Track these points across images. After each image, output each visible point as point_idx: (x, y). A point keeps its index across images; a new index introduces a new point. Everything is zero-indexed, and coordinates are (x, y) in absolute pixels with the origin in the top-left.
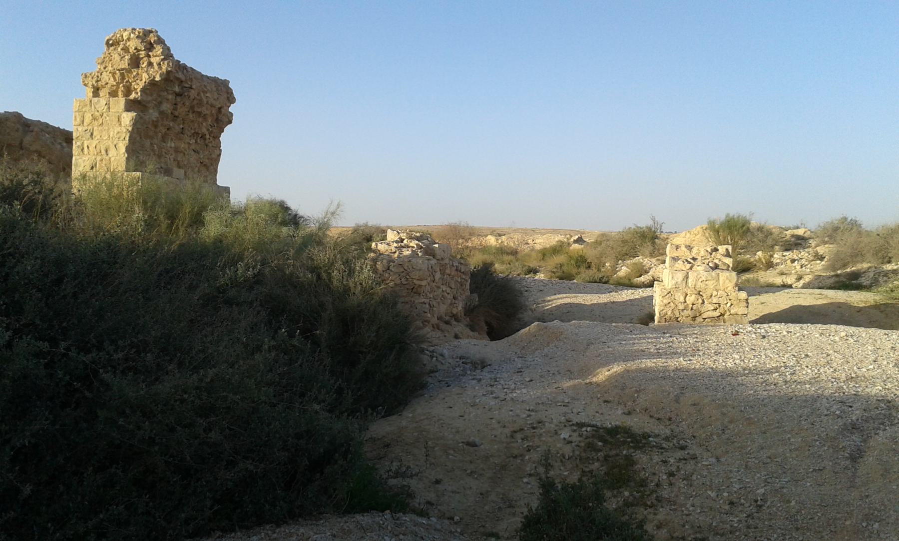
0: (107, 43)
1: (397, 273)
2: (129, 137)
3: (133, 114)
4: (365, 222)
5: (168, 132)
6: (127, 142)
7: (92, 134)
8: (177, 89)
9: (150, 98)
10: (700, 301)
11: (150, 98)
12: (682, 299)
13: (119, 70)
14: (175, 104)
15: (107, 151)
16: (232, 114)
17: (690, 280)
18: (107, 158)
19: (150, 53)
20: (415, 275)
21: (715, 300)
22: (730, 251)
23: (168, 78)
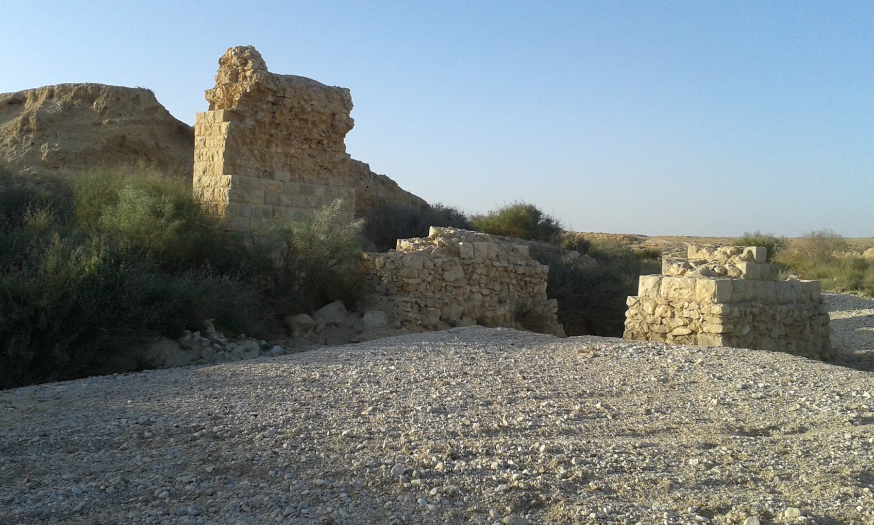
0: (220, 62)
1: (390, 269)
2: (226, 144)
3: (227, 123)
4: (756, 231)
5: (270, 138)
6: (224, 148)
7: (205, 143)
8: (270, 98)
9: (246, 108)
10: (669, 313)
11: (246, 108)
12: (650, 310)
13: (224, 85)
14: (274, 113)
15: (213, 157)
16: (353, 120)
17: (662, 287)
18: (213, 163)
19: (245, 68)
20: (404, 272)
21: (686, 313)
22: (755, 254)
23: (258, 88)
